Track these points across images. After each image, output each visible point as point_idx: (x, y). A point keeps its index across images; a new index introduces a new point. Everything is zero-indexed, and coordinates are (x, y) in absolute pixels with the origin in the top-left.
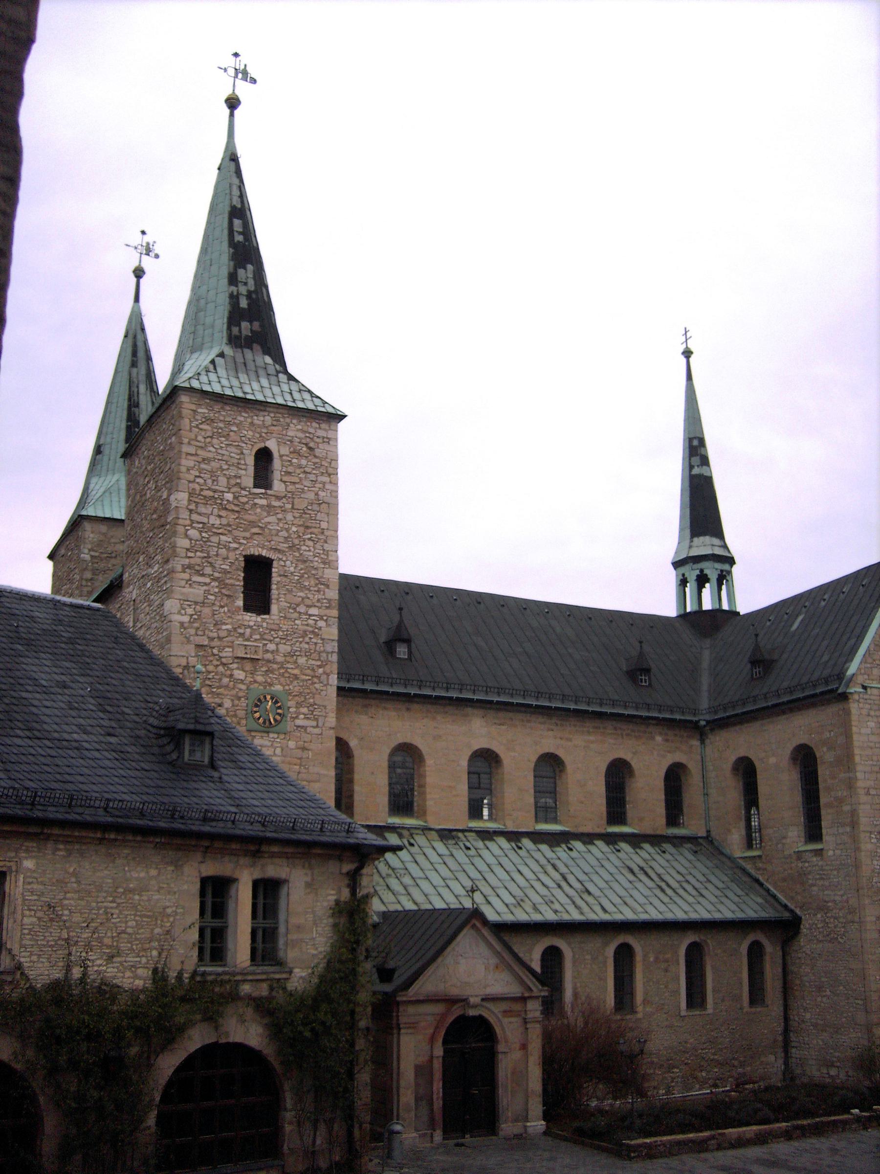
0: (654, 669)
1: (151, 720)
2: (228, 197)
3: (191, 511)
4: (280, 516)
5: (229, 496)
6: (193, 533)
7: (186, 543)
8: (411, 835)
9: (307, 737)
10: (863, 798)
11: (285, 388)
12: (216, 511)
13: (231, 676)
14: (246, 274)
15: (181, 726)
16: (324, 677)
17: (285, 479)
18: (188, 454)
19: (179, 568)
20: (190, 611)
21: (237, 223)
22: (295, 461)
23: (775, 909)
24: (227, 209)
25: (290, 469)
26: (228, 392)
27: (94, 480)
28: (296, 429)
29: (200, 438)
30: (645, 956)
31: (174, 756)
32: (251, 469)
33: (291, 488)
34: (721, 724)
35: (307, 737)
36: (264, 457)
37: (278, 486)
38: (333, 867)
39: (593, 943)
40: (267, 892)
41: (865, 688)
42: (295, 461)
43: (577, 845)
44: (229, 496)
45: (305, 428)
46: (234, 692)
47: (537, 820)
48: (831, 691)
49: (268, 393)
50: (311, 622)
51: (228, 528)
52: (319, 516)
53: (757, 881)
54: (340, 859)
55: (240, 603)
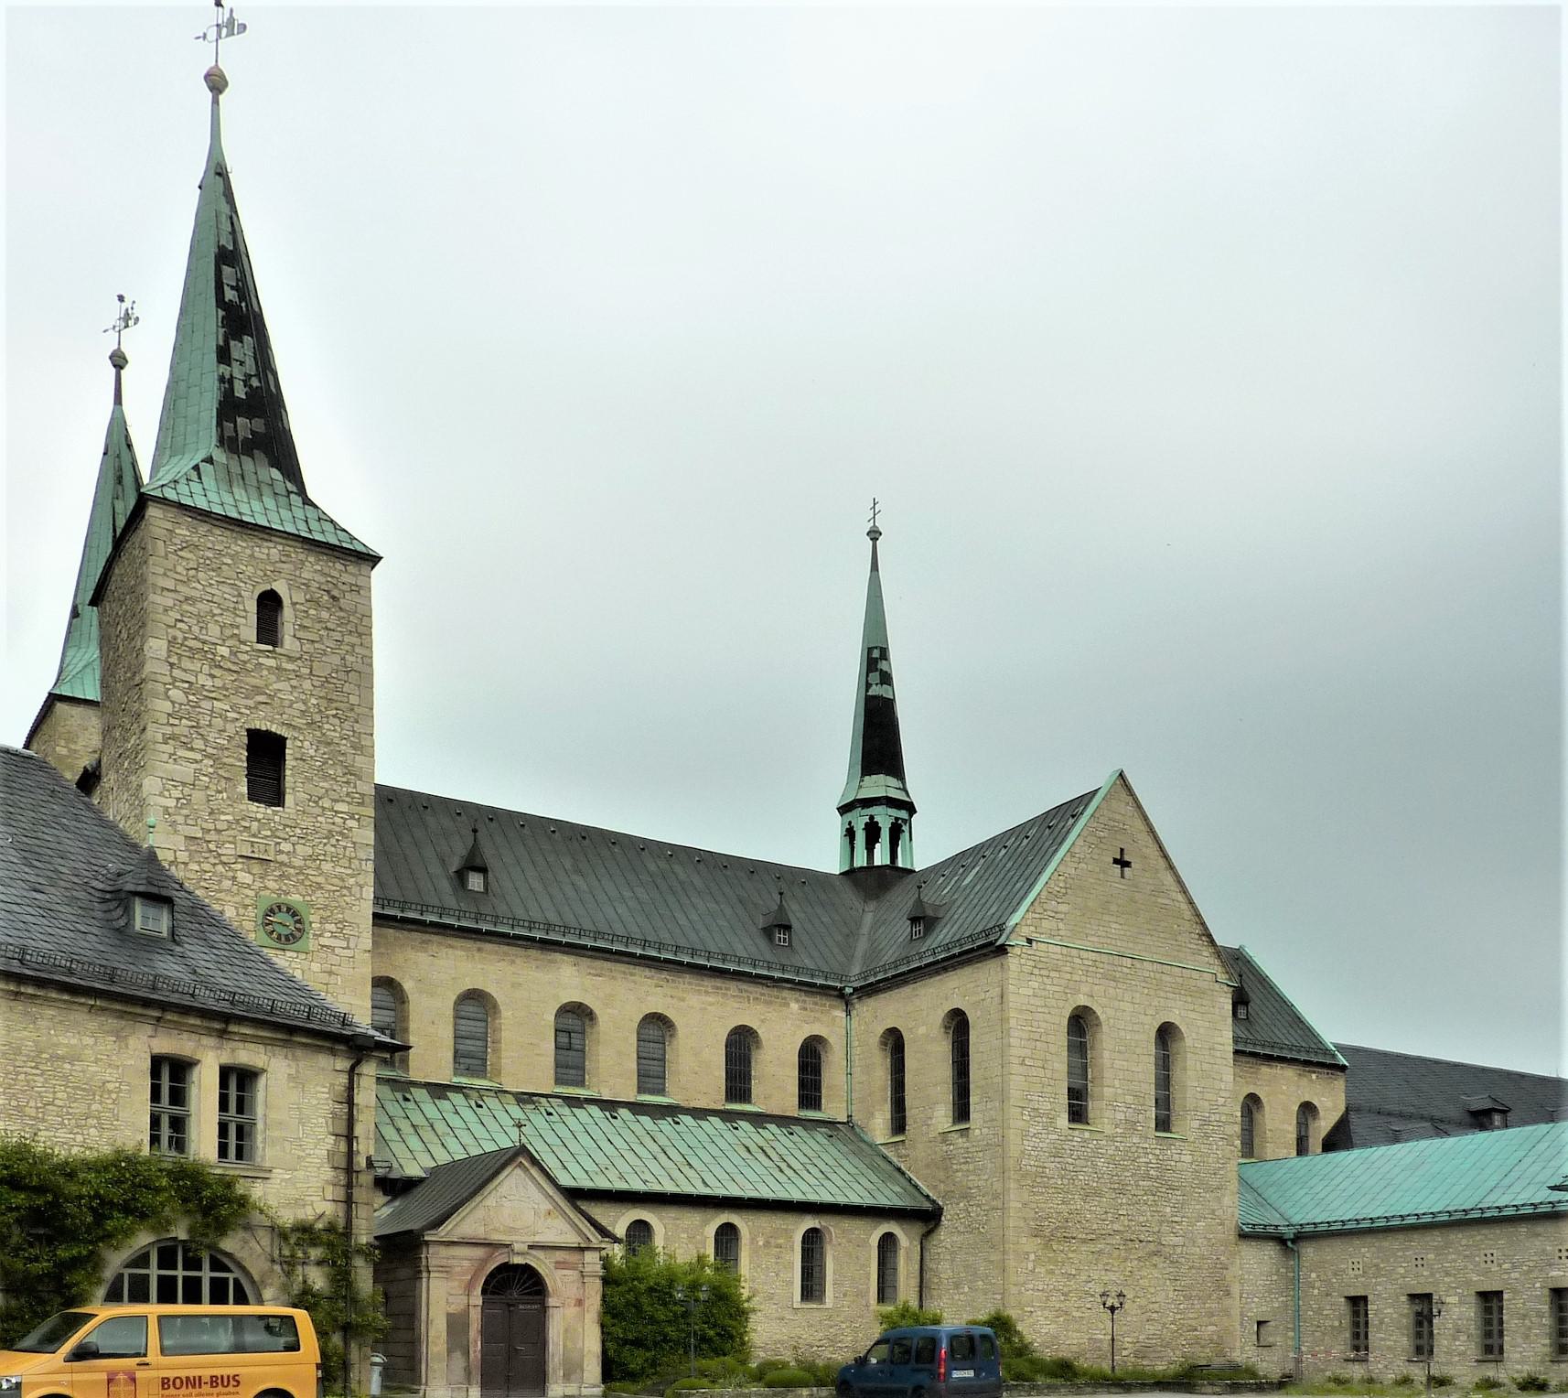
0: (795, 925)
2: (214, 231)
3: (172, 665)
4: (294, 683)
6: (176, 694)
7: (167, 706)
8: (481, 1097)
9: (335, 960)
10: (1016, 1068)
11: (299, 513)
12: (206, 669)
13: (234, 878)
14: (242, 350)
15: (130, 887)
16: (356, 890)
17: (299, 634)
18: (163, 589)
20: (176, 793)
21: (227, 270)
22: (312, 612)
23: (914, 1198)
24: (214, 250)
25: (307, 623)
26: (217, 510)
27: (70, 653)
28: (314, 568)
29: (179, 569)
30: (753, 1240)
31: (122, 922)
33: (307, 647)
34: (869, 990)
35: (335, 960)
36: (269, 604)
37: (289, 643)
38: (324, 1061)
39: (691, 1218)
40: (238, 1081)
41: (1029, 941)
42: (312, 612)
43: (687, 1119)
45: (326, 570)
46: (237, 899)
47: (641, 1090)
48: (991, 944)
50: (337, 820)
53: (899, 1169)
54: (333, 1052)
55: (245, 790)
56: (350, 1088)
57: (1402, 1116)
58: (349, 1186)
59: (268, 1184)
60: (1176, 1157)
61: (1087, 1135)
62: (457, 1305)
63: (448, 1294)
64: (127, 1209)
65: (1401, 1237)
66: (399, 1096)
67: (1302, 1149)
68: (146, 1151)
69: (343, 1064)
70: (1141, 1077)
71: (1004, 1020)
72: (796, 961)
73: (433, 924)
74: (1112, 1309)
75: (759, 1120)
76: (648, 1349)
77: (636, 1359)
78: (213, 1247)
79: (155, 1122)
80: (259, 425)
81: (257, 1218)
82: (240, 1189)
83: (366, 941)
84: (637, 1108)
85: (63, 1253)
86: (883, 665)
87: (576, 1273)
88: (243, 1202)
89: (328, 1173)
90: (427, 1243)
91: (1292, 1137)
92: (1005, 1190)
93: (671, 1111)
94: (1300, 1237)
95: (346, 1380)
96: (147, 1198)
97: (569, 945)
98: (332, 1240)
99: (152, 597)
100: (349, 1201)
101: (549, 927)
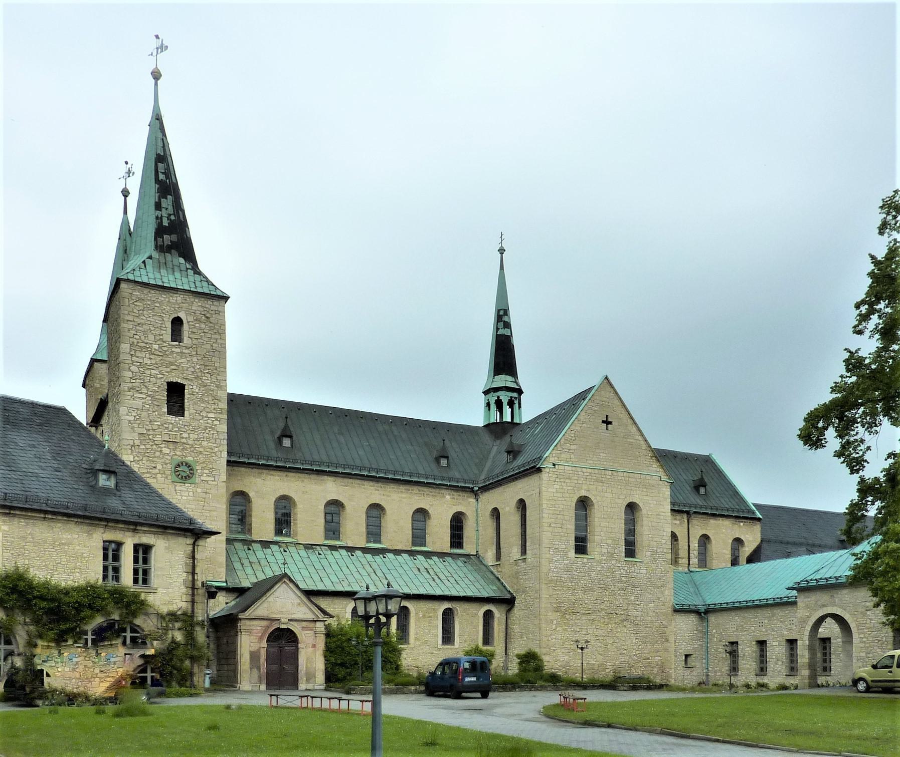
1: (84, 466)
5: (156, 347)
7: (130, 374)
10: (546, 528)
11: (191, 279)
14: (168, 203)
15: (97, 467)
19: (126, 389)
23: (502, 591)
25: (195, 330)
26: (152, 282)
28: (197, 304)
32: (169, 330)
33: (195, 342)
34: (485, 489)
36: (177, 323)
37: (186, 340)
41: (554, 465)
43: (391, 555)
44: (156, 347)
47: (368, 541)
49: (179, 282)
50: (209, 421)
51: (156, 366)
52: (214, 357)
54: (186, 536)
55: (166, 410)
56: (193, 551)
57: (794, 544)
58: (193, 595)
59: (156, 595)
60: (637, 571)
61: (585, 560)
62: (255, 647)
63: (250, 642)
64: (91, 607)
65: (753, 611)
66: (246, 547)
67: (735, 562)
68: (100, 581)
69: (190, 541)
70: (616, 530)
71: (540, 505)
72: (451, 474)
73: (263, 465)
74: (582, 649)
75: (428, 555)
76: (347, 668)
77: (341, 672)
78: (131, 623)
79: (105, 569)
80: (174, 238)
81: (151, 610)
82: (143, 596)
83: (224, 477)
84: (365, 550)
85: (63, 627)
86: (505, 319)
87: (312, 633)
88: (143, 603)
89: (184, 590)
90: (240, 619)
91: (728, 557)
92: (540, 589)
93: (383, 551)
94: (707, 612)
95: (192, 680)
96: (99, 603)
97: (330, 472)
98: (187, 620)
99: (123, 325)
100: (193, 602)
101: (321, 463)
